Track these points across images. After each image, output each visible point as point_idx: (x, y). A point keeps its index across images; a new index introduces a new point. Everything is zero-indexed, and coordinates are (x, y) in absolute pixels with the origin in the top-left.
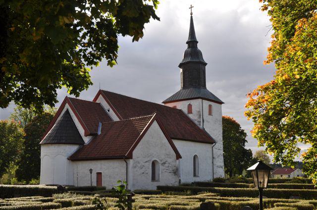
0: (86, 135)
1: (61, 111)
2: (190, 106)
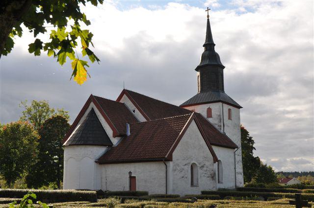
0: (114, 136)
1: (86, 110)
2: (209, 111)
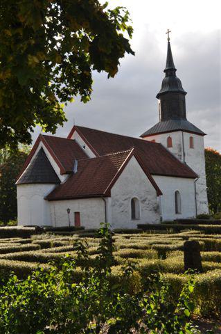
0: (62, 174)
2: (169, 140)
